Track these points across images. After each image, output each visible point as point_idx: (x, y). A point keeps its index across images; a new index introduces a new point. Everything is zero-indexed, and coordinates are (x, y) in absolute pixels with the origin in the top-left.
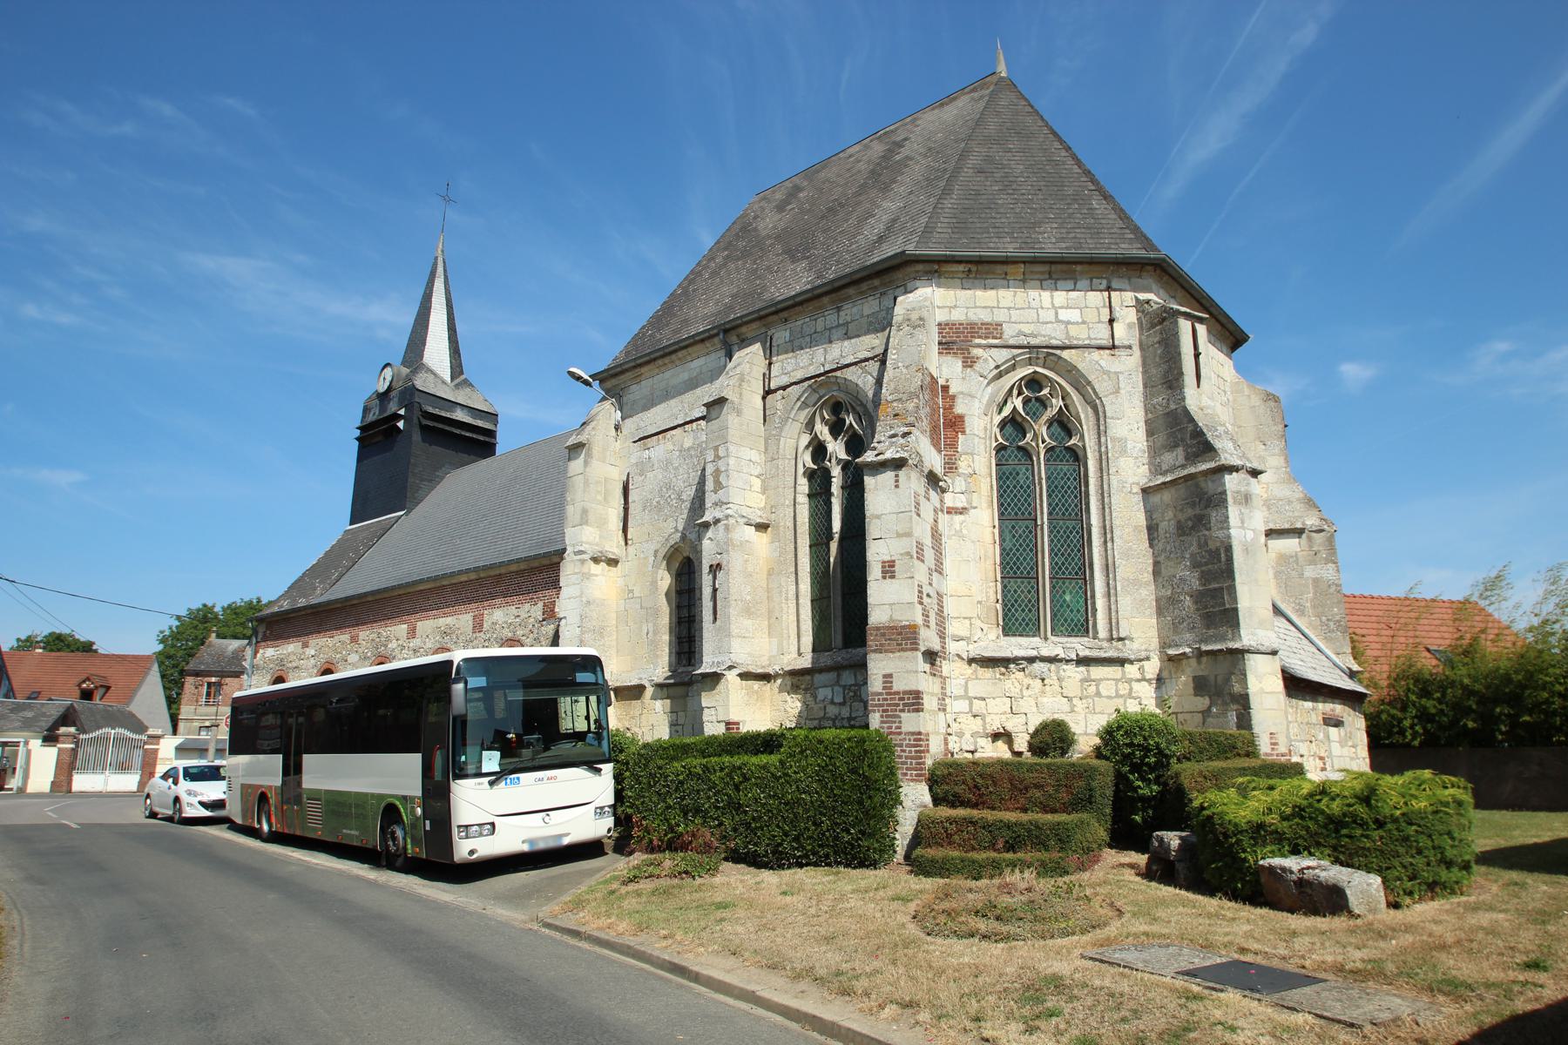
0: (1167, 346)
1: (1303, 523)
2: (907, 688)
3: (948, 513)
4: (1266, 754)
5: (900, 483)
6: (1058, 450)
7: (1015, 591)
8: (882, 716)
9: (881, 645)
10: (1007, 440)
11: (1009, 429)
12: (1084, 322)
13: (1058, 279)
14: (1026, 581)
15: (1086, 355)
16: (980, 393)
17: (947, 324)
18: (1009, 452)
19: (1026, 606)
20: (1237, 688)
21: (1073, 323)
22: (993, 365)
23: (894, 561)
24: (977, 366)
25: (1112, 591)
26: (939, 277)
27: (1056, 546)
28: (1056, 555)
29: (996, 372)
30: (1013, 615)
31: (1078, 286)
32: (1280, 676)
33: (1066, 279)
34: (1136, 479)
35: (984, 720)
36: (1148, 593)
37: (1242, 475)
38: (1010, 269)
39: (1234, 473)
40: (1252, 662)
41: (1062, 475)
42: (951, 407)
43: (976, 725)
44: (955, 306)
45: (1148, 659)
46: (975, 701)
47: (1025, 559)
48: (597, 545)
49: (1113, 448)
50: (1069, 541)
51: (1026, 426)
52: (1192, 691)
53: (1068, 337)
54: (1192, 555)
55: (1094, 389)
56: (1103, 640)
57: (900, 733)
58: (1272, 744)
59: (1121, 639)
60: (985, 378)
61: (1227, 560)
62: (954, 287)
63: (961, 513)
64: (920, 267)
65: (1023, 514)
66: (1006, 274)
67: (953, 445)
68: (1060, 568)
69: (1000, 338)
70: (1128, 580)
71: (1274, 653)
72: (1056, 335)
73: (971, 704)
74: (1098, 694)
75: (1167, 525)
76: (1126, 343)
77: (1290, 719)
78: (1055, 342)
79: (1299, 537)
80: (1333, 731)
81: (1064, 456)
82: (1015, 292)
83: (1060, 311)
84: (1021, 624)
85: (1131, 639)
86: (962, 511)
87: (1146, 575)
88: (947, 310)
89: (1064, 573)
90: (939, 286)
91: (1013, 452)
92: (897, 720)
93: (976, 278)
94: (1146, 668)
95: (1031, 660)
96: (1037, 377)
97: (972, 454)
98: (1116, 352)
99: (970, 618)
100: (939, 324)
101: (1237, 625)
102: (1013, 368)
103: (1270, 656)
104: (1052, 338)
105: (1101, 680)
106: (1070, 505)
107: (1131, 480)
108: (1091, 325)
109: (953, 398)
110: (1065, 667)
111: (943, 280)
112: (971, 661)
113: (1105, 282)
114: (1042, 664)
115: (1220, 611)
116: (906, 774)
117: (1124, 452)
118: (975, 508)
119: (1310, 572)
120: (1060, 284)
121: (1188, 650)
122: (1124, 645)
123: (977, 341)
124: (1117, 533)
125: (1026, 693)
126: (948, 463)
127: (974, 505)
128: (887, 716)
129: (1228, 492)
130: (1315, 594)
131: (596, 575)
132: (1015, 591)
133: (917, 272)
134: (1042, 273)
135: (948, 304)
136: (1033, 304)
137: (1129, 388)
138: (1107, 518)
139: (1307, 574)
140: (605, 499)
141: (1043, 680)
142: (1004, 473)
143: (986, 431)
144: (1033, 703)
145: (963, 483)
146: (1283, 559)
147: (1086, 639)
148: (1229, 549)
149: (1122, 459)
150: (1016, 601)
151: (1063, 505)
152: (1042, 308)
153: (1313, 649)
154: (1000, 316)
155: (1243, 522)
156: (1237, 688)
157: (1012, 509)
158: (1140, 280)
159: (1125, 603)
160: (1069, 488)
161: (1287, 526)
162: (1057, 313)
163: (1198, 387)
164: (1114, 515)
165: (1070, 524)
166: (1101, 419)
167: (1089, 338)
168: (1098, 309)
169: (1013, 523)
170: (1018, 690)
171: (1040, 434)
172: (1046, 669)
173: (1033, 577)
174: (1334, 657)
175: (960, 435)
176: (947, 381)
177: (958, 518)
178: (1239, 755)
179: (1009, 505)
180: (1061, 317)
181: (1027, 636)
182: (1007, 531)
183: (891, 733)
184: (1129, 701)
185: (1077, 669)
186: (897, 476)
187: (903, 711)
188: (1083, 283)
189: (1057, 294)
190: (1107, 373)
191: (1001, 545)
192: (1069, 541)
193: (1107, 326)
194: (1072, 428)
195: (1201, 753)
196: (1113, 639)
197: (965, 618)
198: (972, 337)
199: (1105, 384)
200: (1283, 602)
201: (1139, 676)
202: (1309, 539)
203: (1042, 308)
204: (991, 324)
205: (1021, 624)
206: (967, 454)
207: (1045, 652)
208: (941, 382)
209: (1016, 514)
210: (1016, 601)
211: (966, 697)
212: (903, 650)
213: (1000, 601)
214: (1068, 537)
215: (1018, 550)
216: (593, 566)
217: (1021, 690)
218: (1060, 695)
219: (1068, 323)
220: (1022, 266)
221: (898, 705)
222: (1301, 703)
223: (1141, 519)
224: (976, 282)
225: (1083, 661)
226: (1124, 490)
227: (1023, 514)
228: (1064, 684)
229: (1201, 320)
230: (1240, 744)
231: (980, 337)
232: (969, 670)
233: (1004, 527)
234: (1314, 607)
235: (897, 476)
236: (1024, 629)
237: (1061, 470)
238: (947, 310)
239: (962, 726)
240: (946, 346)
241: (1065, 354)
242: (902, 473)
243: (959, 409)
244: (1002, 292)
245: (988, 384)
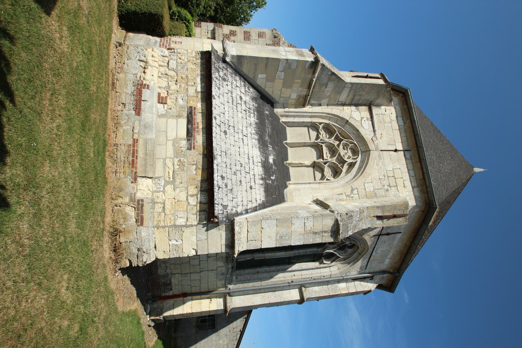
163: (352, 77)
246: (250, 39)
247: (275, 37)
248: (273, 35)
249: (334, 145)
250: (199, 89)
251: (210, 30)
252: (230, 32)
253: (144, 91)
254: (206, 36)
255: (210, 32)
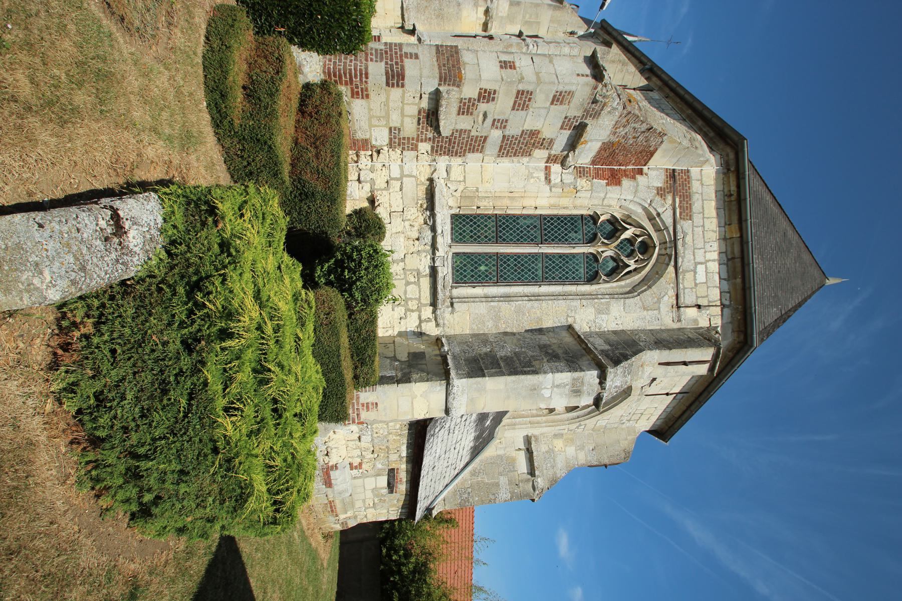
0: (688, 341)
1: (539, 476)
2: (406, 68)
3: (546, 167)
4: (358, 398)
5: (581, 78)
6: (595, 265)
7: (486, 226)
8: (381, 50)
9: (443, 54)
10: (601, 225)
11: (609, 228)
12: (696, 285)
13: (727, 266)
14: (494, 234)
15: (672, 285)
16: (638, 200)
17: (688, 177)
18: (592, 226)
19: (475, 234)
20: (415, 376)
21: (695, 276)
22: (660, 210)
23: (515, 68)
24: (658, 198)
25: (490, 299)
26: (724, 174)
27: (522, 260)
28: (515, 260)
29: (654, 213)
30: (467, 223)
31: (723, 281)
32: (428, 416)
33: (728, 272)
34: (578, 321)
35: (385, 189)
36: (490, 328)
37: (596, 388)
38: (735, 226)
39: (598, 380)
40: (439, 388)
41: (577, 267)
42: (626, 176)
43: (380, 183)
44: (702, 185)
45: (437, 325)
46: (399, 183)
47: (511, 234)
48: (497, 14)
49: (601, 303)
50: (526, 270)
51: (613, 240)
52: (412, 351)
53: (685, 272)
54: (525, 352)
55: (645, 290)
56: (450, 292)
57: (366, 60)
58: (367, 404)
59: (452, 304)
60: (650, 205)
61: (525, 372)
62: (716, 184)
63: (546, 178)
64: (732, 156)
65: (546, 235)
66: (729, 225)
67: (598, 175)
68: (505, 263)
69: (681, 218)
70: (499, 312)
71: (447, 411)
72: (685, 262)
73: (396, 179)
74: (408, 283)
75: (545, 339)
76: (683, 317)
77: (390, 424)
78: (680, 260)
79: (528, 473)
80: (383, 481)
81: (590, 270)
82: (716, 232)
83: (703, 266)
84: (460, 229)
85: (452, 313)
86: (548, 179)
87: (504, 326)
88: (699, 177)
89: (501, 265)
90: (717, 172)
91: (592, 229)
92: (379, 60)
93: (725, 201)
94: (430, 324)
95: (433, 229)
96: (651, 250)
97: (591, 190)
98: (675, 309)
99: (464, 181)
100: (688, 171)
101: (469, 376)
102: (658, 230)
103: (444, 408)
104: (683, 259)
105: (419, 286)
106: (553, 273)
107: (577, 317)
108: (694, 290)
109: (634, 178)
110: (429, 257)
111: (721, 176)
112: (431, 180)
113: (727, 303)
114: (430, 238)
115: (481, 367)
116: (330, 61)
117: (599, 312)
118: (551, 190)
119: (503, 480)
120: (724, 267)
121: (446, 348)
122: (448, 307)
123: (677, 200)
124: (536, 304)
125: (407, 223)
126: (584, 171)
127: (553, 189)
128: (382, 54)
129: (583, 373)
130: (487, 484)
131: (477, 13)
132: (486, 226)
133: (727, 155)
134: (733, 252)
135: (704, 179)
136: (708, 246)
137: (648, 318)
138: (547, 298)
139: (502, 478)
140: (526, 22)
141: (418, 239)
142: (576, 222)
143: (608, 206)
144: (400, 229)
145: (570, 181)
146: (512, 462)
147: (451, 281)
148: (535, 372)
149: (593, 310)
150: (479, 226)
151: (554, 267)
152: (705, 252)
153: (447, 481)
154: (697, 219)
155: (558, 386)
156: (415, 376)
157: (549, 227)
158: (731, 331)
159: (481, 308)
160: (567, 273)
161: (536, 464)
162: (701, 263)
163: (659, 364)
164: (550, 302)
165: (540, 273)
166: (623, 296)
167: (684, 288)
168: (707, 296)
169: (539, 227)
170: (409, 217)
171: (607, 251)
172: (426, 241)
173: (498, 239)
174: (442, 497)
175: (605, 181)
176: (646, 174)
177: (542, 176)
178: (356, 368)
179: (552, 224)
180: (699, 267)
181: (452, 234)
182: (532, 221)
183: (367, 54)
184: (403, 309)
185: (427, 267)
186: (587, 76)
187: (386, 63)
188: (726, 286)
189: (716, 264)
190: (659, 301)
191: (521, 216)
192: (526, 270)
193: (694, 303)
194: (613, 276)
195: (356, 331)
196: (452, 299)
197: (465, 177)
198: (680, 196)
199: (650, 299)
200: (480, 461)
201: (423, 318)
202: (528, 480)
203: (705, 252)
204: (691, 212)
205: (460, 229)
206: (592, 186)
207: (439, 239)
208: (645, 168)
209: (545, 229)
210: (479, 226)
211: (403, 175)
212: (440, 68)
213: (479, 212)
214: (529, 270)
215: (518, 229)
216: (482, 10)
217: (409, 220)
218: (405, 252)
219: (695, 273)
220: (738, 235)
221: (392, 60)
222: (405, 441)
223: (548, 324)
224: (722, 202)
225: (434, 271)
226: (569, 311)
227: (546, 235)
228: (415, 255)
229: (711, 369)
230: (365, 369)
231: (680, 202)
232: (423, 178)
233: (535, 219)
234: (478, 483)
235: (587, 76)
236: (457, 231)
237: (580, 267)
238: (699, 177)
239: (379, 172)
240: (672, 175)
241: (671, 269)
242: (591, 80)
243: (626, 182)
244: (715, 221)
245: (645, 209)
246: (527, 107)
247: (595, 101)
248: (593, 97)
249: (645, 165)
250: (404, 454)
251: (427, 93)
252: (480, 94)
253: (332, 473)
254: (416, 104)
255: (426, 97)
